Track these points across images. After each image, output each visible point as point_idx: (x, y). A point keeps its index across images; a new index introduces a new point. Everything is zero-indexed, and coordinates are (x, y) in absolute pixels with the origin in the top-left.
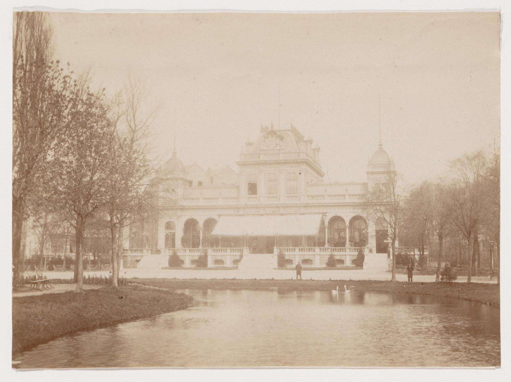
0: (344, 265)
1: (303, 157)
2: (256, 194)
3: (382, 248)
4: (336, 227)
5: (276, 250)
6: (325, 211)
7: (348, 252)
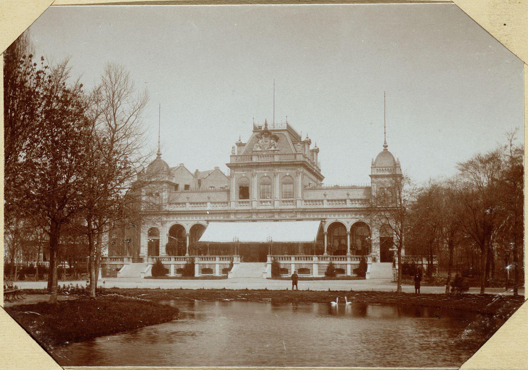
1: (300, 158)
3: (386, 257)
5: (269, 260)
6: (324, 217)
7: (349, 261)
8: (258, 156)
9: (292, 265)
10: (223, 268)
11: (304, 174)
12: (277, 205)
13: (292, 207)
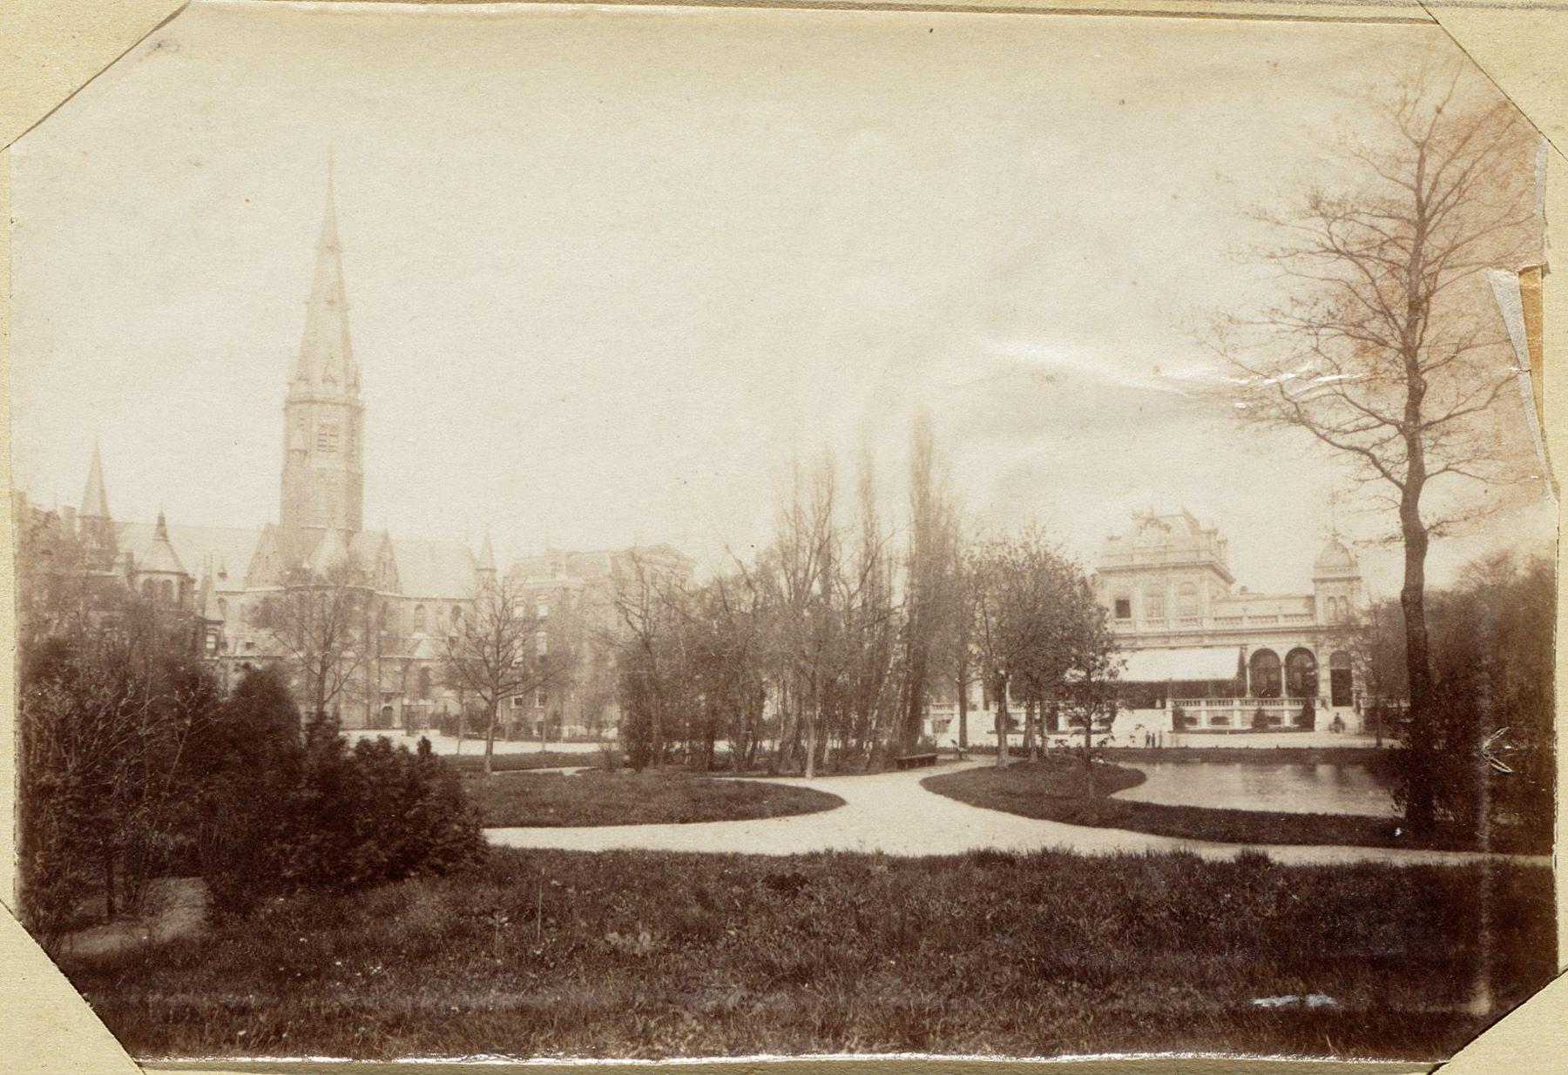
0: (1282, 726)
1: (1205, 557)
2: (1129, 616)
3: (1341, 697)
4: (1261, 665)
6: (1244, 641)
7: (1286, 706)
8: (1142, 555)
9: (1235, 712)
10: (1211, 716)
11: (1211, 579)
12: (1174, 627)
13: (1196, 628)
